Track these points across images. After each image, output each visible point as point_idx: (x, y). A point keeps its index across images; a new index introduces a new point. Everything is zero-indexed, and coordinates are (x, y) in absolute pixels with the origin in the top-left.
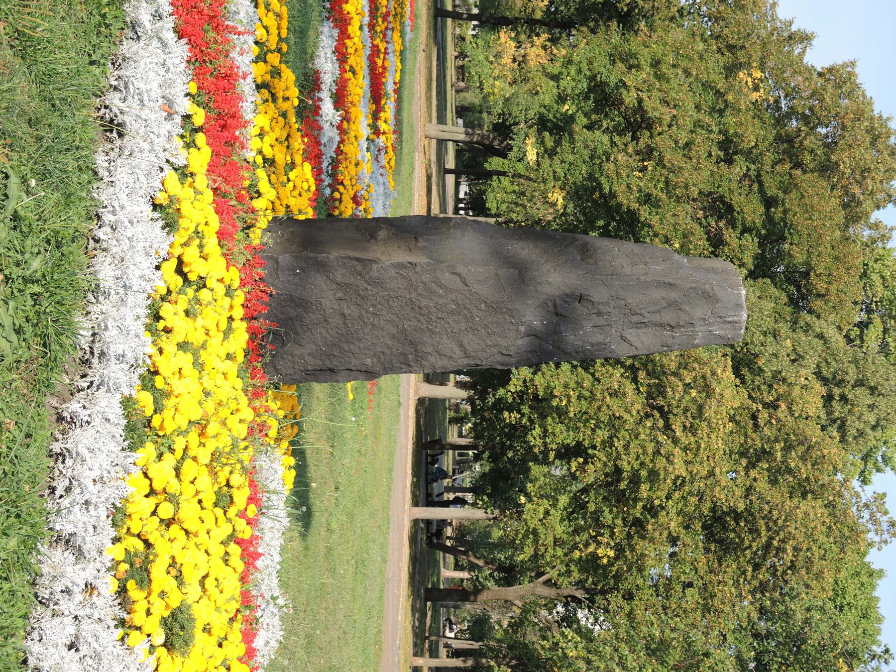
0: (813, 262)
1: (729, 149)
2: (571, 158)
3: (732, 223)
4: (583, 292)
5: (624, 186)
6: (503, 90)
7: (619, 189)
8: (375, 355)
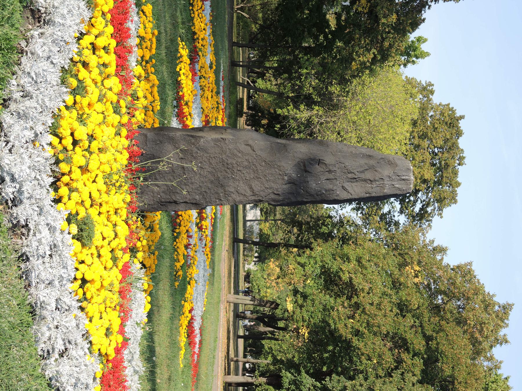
0: (456, 375)
1: (402, 308)
2: (312, 309)
3: (407, 350)
4: (321, 158)
5: (343, 325)
6: (272, 294)
7: (340, 326)
8: (201, 194)
